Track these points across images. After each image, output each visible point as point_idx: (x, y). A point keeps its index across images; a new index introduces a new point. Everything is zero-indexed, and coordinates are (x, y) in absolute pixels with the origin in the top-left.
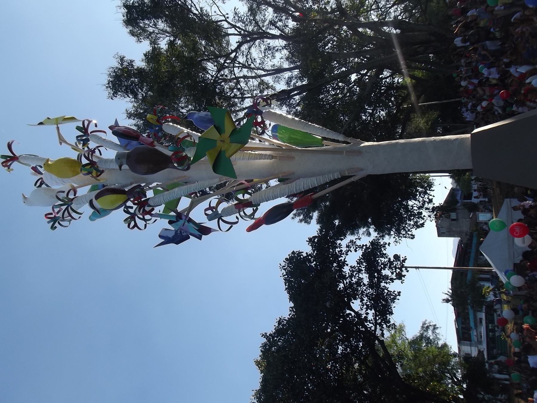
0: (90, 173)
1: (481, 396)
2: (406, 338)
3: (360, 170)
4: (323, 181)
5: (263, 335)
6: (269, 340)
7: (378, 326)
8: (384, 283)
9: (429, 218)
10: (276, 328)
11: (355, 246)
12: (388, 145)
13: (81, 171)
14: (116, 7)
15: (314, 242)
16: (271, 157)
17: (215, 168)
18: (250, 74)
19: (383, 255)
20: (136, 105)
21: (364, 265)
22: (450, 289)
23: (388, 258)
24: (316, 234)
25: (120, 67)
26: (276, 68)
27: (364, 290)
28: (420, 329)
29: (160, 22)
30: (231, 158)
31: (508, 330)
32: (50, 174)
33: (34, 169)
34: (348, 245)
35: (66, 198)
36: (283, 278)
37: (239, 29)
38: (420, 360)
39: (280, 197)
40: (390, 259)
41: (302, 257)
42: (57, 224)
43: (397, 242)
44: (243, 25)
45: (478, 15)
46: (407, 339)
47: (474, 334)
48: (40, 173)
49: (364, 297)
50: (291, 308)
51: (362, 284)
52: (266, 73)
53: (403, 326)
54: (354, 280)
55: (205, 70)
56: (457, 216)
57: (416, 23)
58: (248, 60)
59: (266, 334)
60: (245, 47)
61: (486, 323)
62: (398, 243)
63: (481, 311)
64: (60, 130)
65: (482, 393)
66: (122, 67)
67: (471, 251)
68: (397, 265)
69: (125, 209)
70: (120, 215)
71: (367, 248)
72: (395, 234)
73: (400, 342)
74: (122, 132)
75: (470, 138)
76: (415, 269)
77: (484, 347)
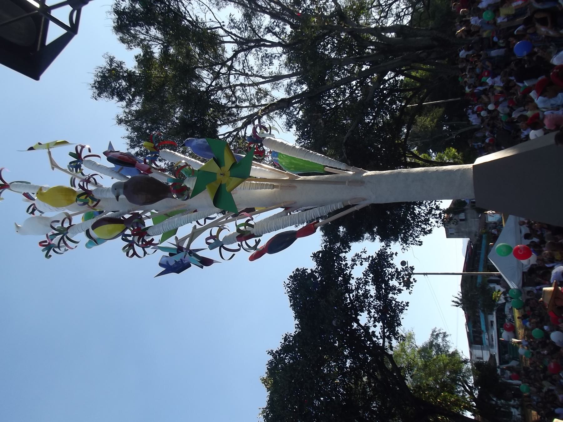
0: (85, 203)
3: (363, 200)
4: (325, 211)
5: (269, 352)
7: (386, 339)
8: (392, 294)
9: (436, 224)
10: (282, 345)
11: (360, 260)
12: (390, 175)
14: (106, 12)
16: (272, 186)
17: (216, 202)
19: (390, 265)
21: (371, 277)
22: (460, 293)
23: (395, 268)
24: (320, 249)
25: (109, 68)
26: (275, 74)
27: (371, 301)
29: (152, 28)
31: (519, 335)
33: (26, 195)
34: (353, 258)
36: (287, 294)
37: (235, 37)
38: (430, 369)
39: (283, 228)
40: (397, 269)
42: (51, 252)
43: (404, 249)
44: (239, 32)
45: (480, 25)
47: (486, 338)
49: (372, 309)
50: (296, 325)
51: (369, 296)
52: (264, 80)
53: (412, 333)
54: (361, 292)
55: (199, 79)
56: (465, 216)
57: (419, 28)
58: (244, 68)
59: (272, 351)
60: (241, 55)
61: (497, 326)
62: (406, 250)
64: (51, 155)
65: (495, 399)
66: (110, 68)
67: (480, 253)
73: (409, 351)
74: (117, 158)
75: (472, 168)
77: (495, 351)
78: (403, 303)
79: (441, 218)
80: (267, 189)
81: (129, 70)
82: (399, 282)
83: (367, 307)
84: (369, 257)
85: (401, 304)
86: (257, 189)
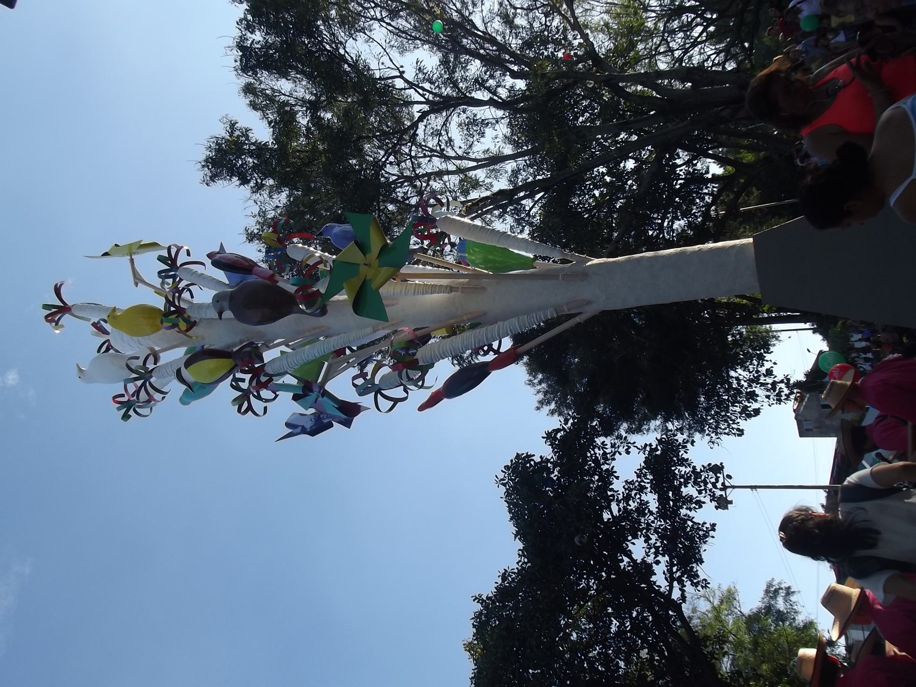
0: (175, 325)
2: (741, 612)
3: (587, 304)
5: (476, 598)
6: (486, 607)
7: (675, 584)
8: (686, 509)
13: (162, 322)
15: (555, 438)
16: (449, 288)
18: (443, 166)
19: (684, 462)
20: (260, 220)
27: (650, 521)
28: (761, 594)
30: (380, 291)
32: (121, 332)
35: (141, 368)
40: (694, 468)
41: (532, 463)
42: (131, 412)
43: (713, 443)
46: (743, 615)
48: (105, 332)
49: (652, 534)
51: (646, 512)
52: (475, 164)
54: (633, 505)
62: (715, 444)
68: (707, 478)
69: (234, 383)
70: (225, 392)
71: (653, 450)
72: (710, 429)
76: (749, 489)
78: (705, 525)
79: (774, 391)
80: (441, 293)
81: (259, 141)
82: (698, 489)
83: (645, 531)
84: (646, 445)
85: (703, 526)
86: (426, 294)
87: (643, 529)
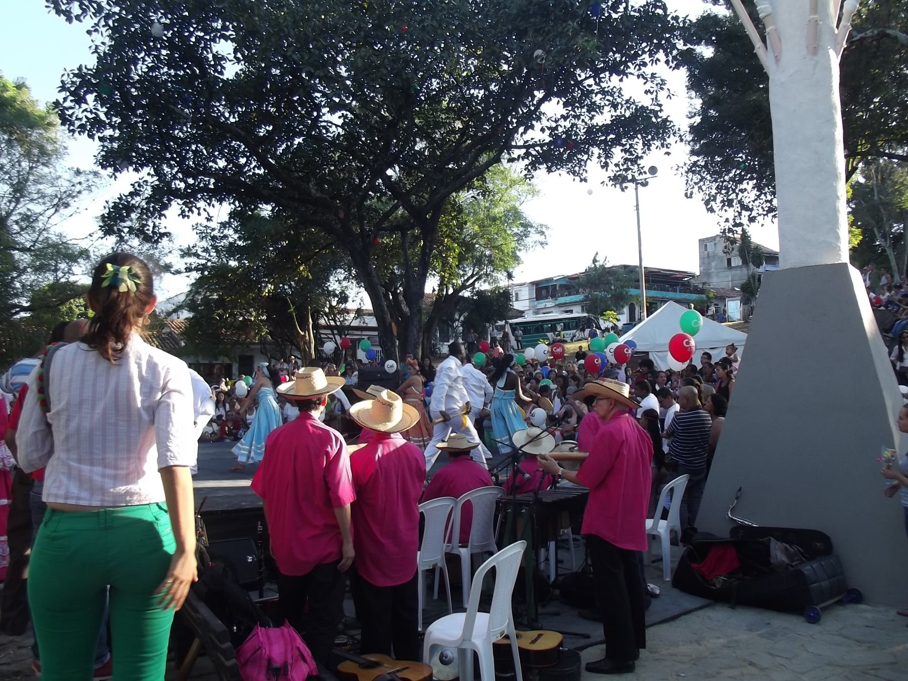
1: (457, 317)
7: (524, 151)
12: (832, 107)
19: (647, 145)
38: (490, 226)
40: (641, 157)
51: (593, 113)
54: (597, 99)
63: (583, 311)
77: (529, 317)
79: (733, 226)
83: (573, 113)
84: (660, 105)
87: (575, 112)
